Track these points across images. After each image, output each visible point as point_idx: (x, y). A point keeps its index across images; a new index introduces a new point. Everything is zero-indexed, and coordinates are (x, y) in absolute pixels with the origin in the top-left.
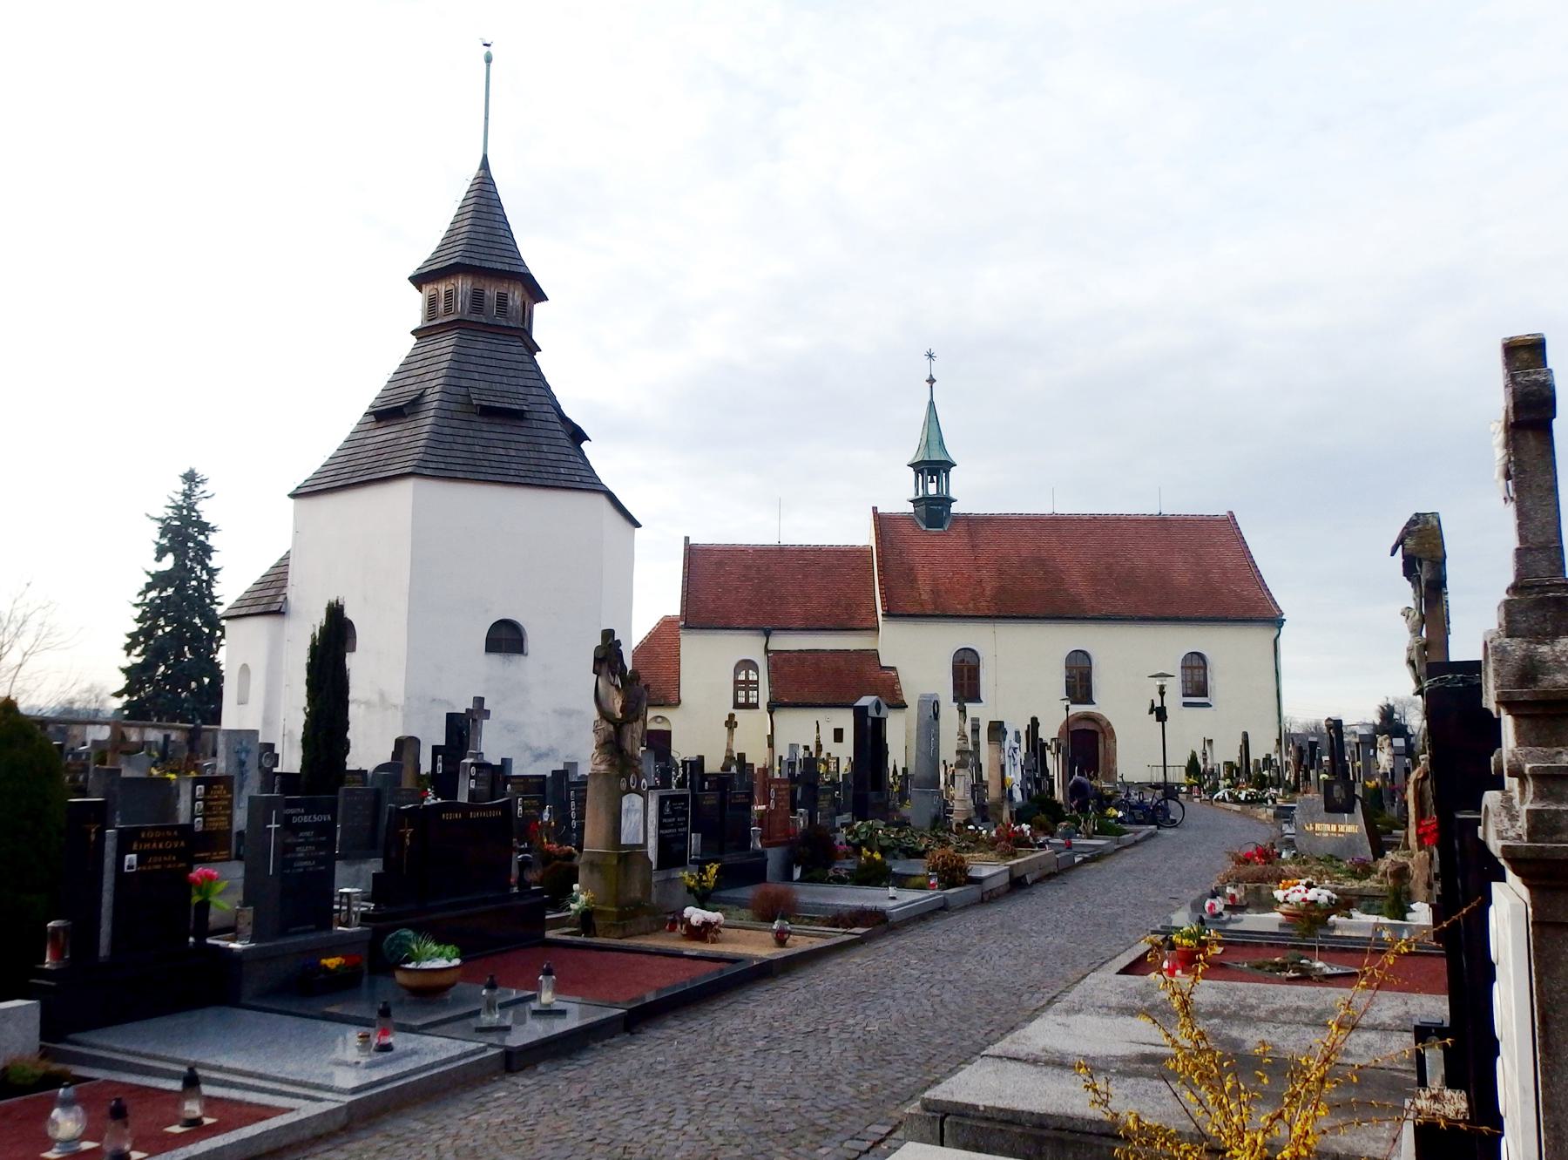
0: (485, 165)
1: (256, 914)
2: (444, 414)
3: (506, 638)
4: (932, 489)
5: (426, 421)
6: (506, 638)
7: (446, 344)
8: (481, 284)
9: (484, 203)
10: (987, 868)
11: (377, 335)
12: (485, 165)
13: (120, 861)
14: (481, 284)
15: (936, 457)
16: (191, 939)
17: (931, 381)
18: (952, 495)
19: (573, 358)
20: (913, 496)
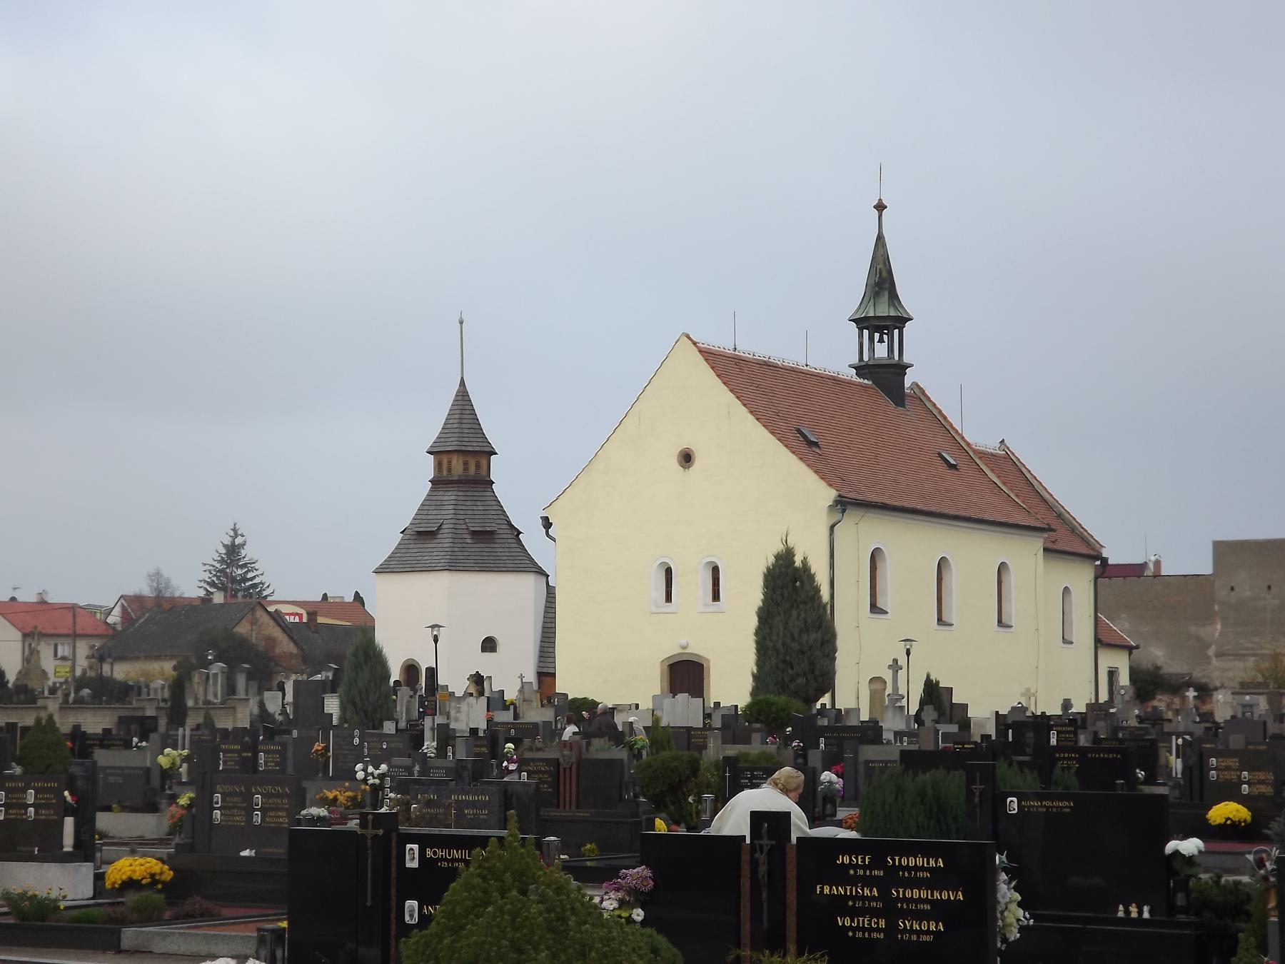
0: (462, 383)
1: (1183, 762)
2: (456, 537)
3: (489, 645)
4: (881, 351)
5: (445, 539)
6: (489, 645)
7: (450, 496)
8: (463, 460)
9: (463, 406)
10: (978, 788)
11: (409, 484)
12: (462, 383)
13: (1250, 853)
14: (463, 460)
15: (884, 310)
16: (246, 853)
17: (880, 207)
18: (907, 359)
19: (515, 488)
20: (855, 360)
